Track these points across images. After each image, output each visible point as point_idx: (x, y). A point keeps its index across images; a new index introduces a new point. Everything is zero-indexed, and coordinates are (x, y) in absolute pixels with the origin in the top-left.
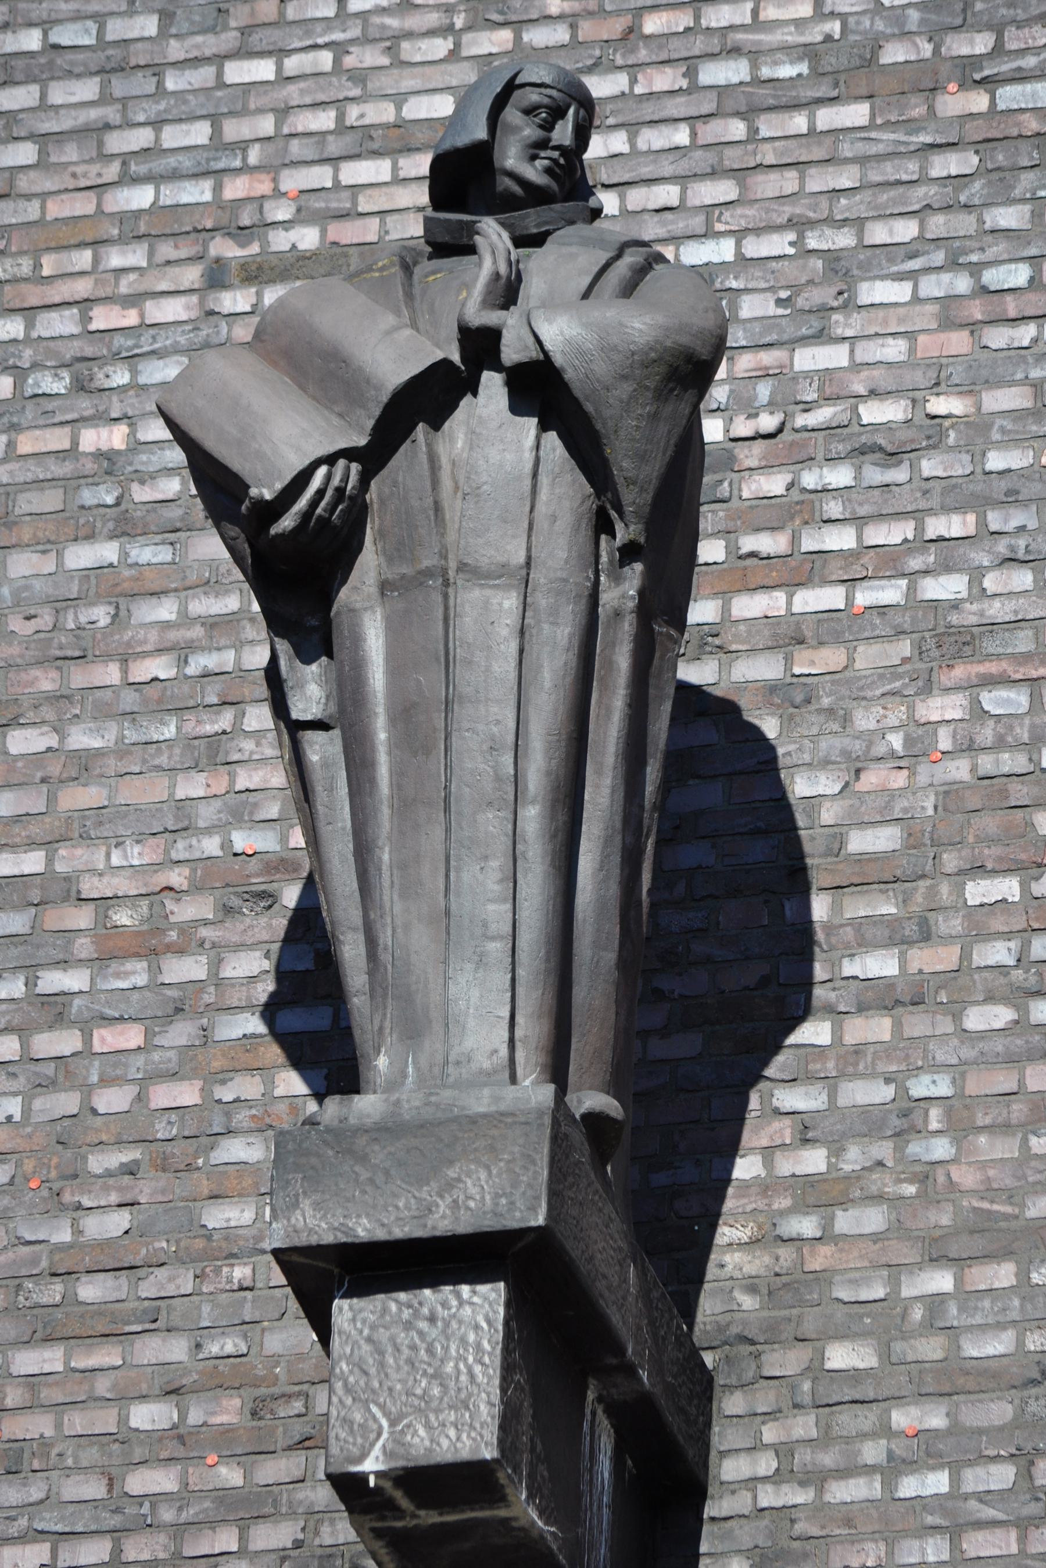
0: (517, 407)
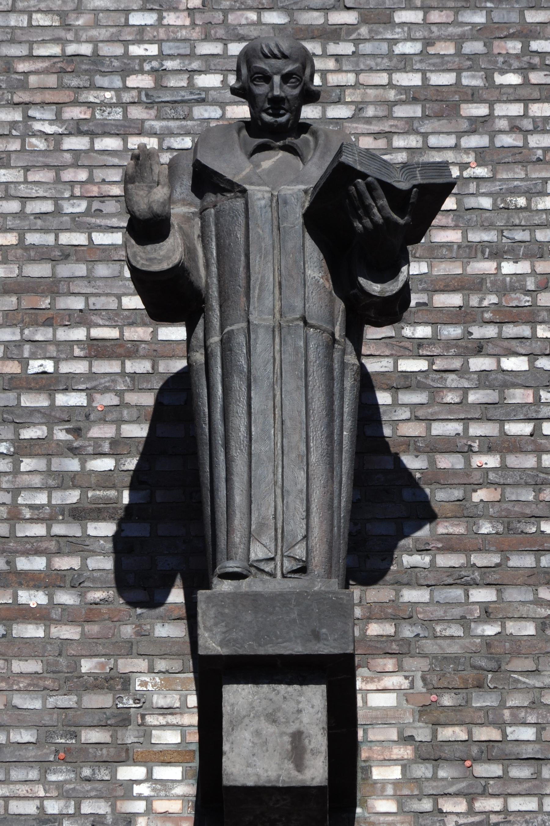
0: (133, 183)
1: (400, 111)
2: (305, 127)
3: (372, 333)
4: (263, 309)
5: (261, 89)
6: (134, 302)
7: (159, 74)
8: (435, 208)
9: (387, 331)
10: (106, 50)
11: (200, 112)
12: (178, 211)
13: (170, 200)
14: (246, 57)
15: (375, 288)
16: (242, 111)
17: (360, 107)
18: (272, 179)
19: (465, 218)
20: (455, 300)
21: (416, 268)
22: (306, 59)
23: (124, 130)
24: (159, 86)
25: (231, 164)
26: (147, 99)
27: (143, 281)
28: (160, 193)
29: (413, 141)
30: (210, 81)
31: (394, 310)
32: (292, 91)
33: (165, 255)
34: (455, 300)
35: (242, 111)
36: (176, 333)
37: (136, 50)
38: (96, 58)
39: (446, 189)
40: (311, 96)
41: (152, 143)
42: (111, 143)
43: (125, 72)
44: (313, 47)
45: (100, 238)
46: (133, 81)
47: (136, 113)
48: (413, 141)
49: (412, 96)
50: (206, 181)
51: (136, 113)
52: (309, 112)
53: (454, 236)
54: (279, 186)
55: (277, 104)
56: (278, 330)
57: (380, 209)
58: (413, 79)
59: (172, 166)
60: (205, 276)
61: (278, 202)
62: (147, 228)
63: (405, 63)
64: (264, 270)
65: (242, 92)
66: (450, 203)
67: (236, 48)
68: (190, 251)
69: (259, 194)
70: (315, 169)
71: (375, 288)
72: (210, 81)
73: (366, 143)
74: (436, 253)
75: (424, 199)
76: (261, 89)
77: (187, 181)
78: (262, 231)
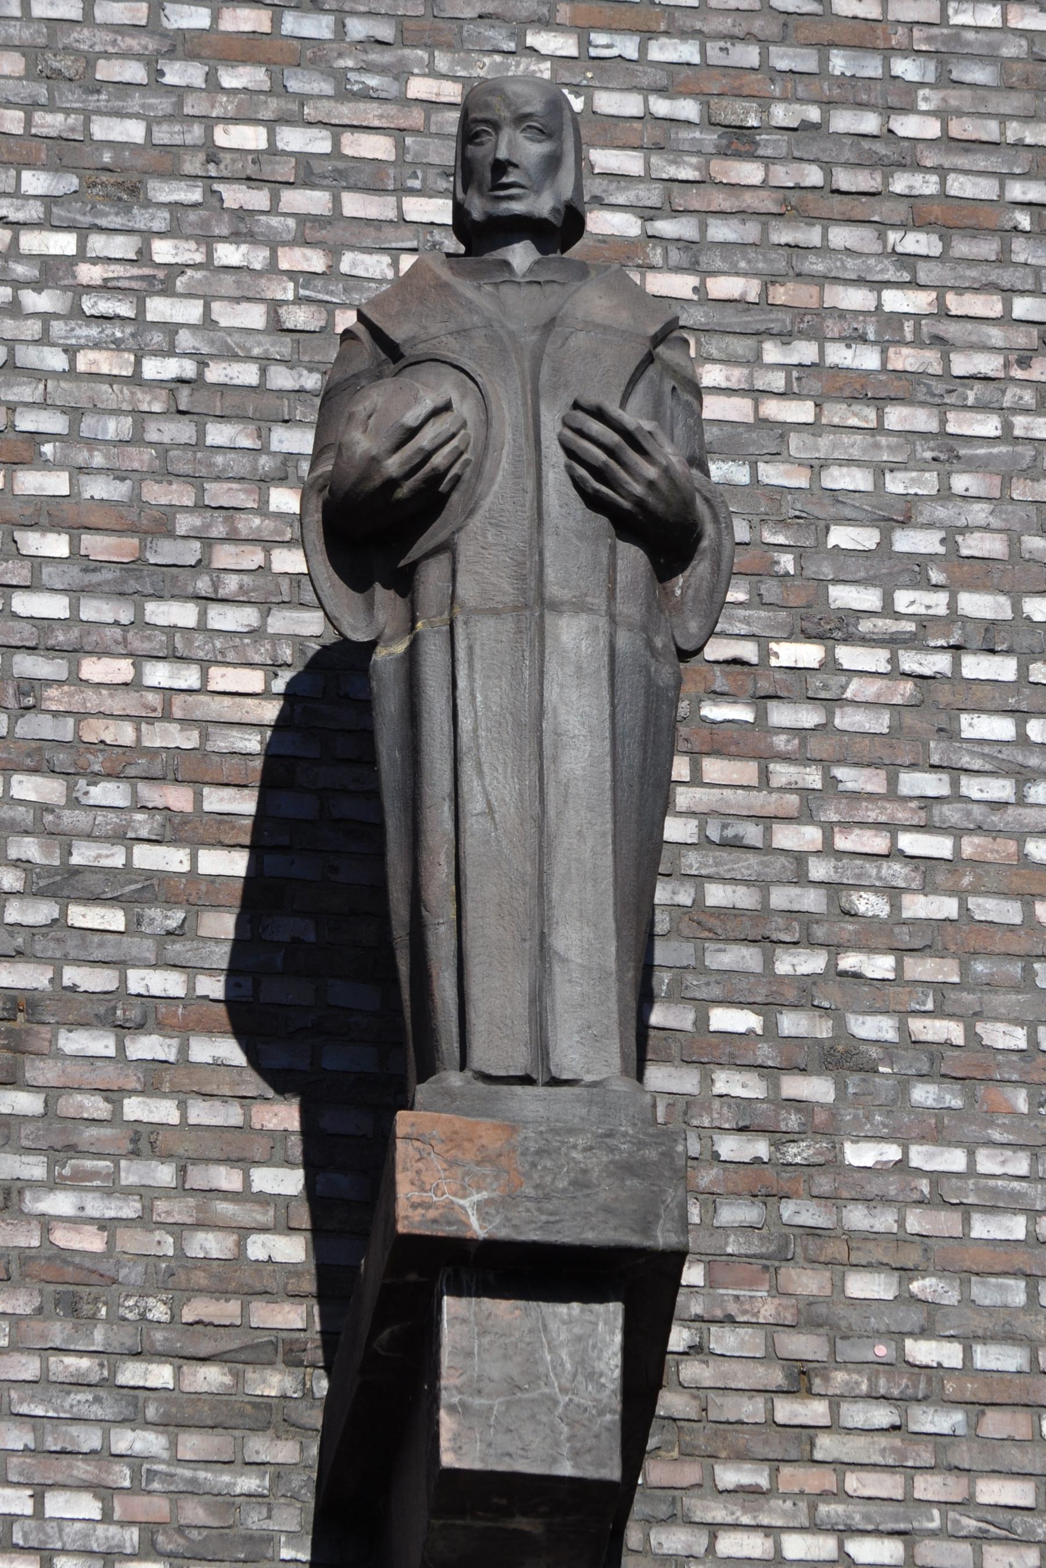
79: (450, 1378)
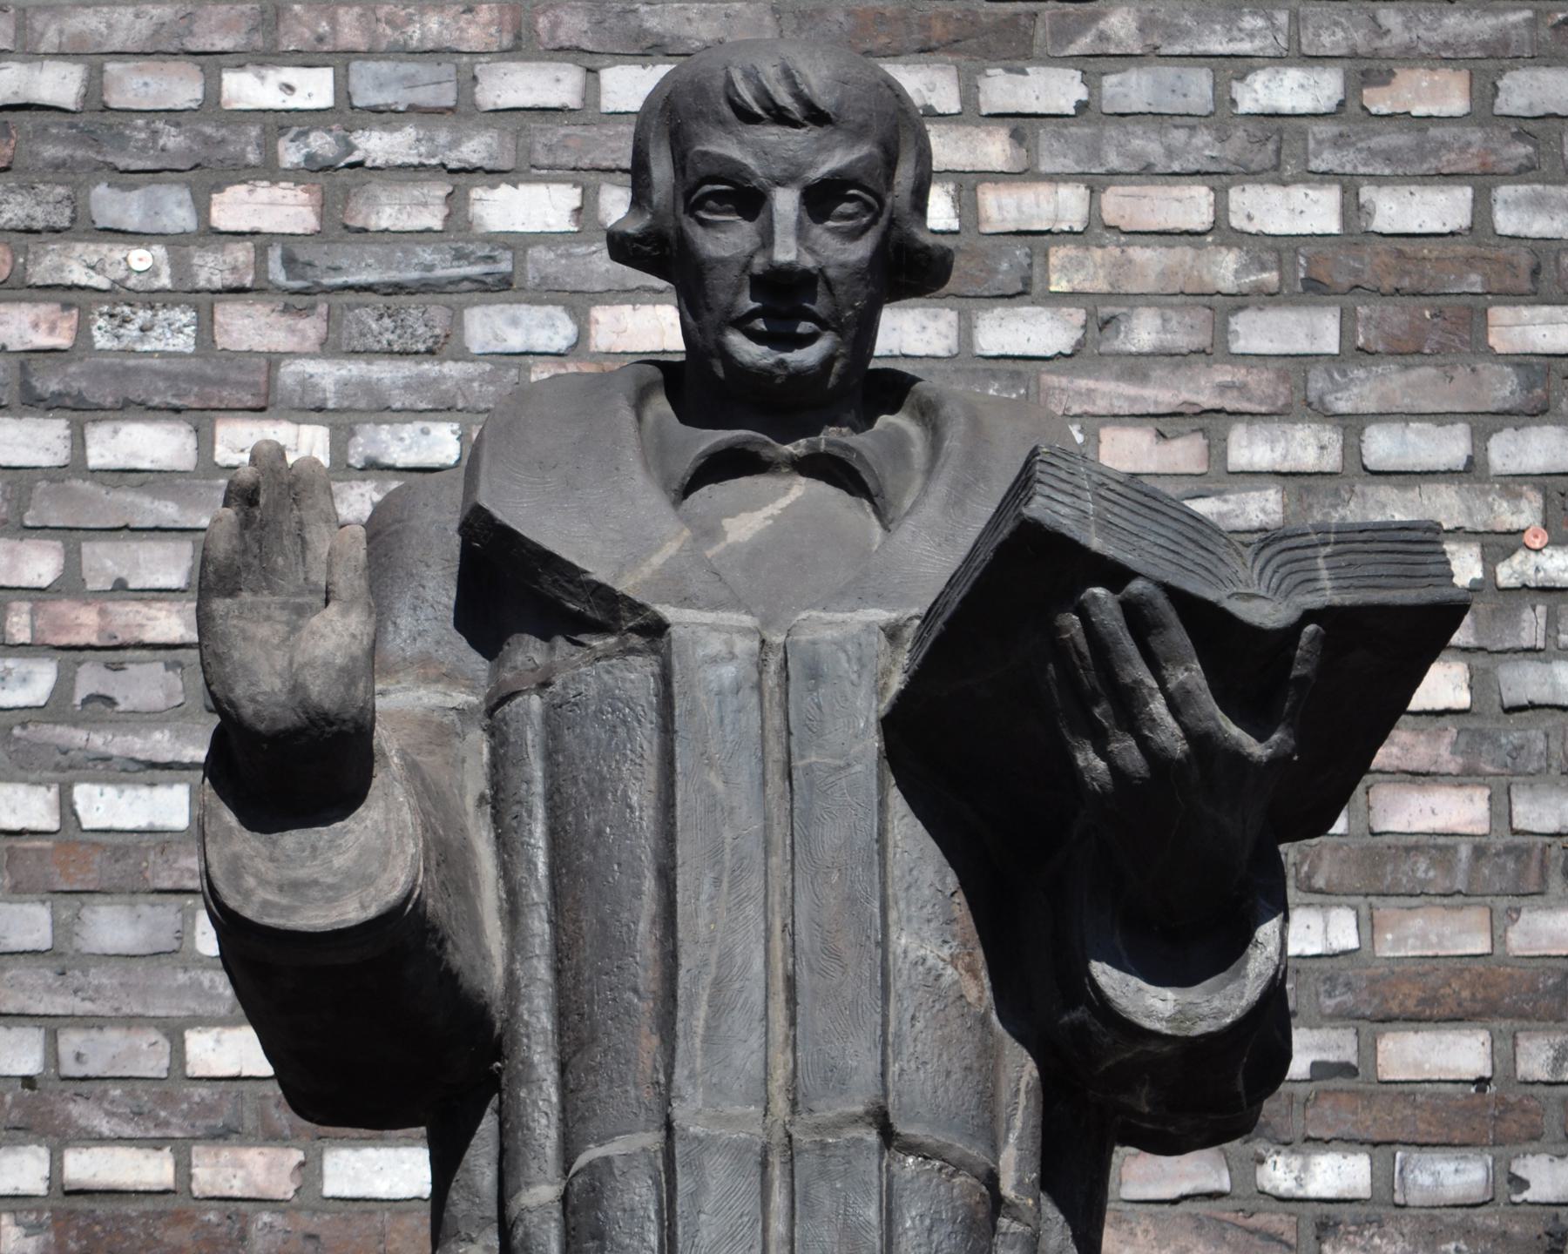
1: (1258, 333)
2: (891, 389)
3: (1139, 1175)
4: (725, 1082)
5: (724, 240)
6: (233, 1051)
7: (337, 178)
8: (1387, 703)
9: (1198, 1171)
10: (135, 87)
11: (493, 327)
12: (402, 705)
13: (371, 661)
14: (670, 116)
15: (1153, 1005)
16: (653, 326)
17: (1102, 315)
18: (760, 581)
19: (1496, 741)
20: (1462, 1054)
21: (1314, 931)
22: (899, 129)
23: (196, 395)
24: (338, 228)
25: (612, 524)
26: (293, 277)
27: (269, 970)
28: (335, 634)
29: (1307, 447)
30: (531, 208)
31: (1222, 1089)
32: (842, 251)
33: (342, 874)
34: (1462, 1054)
35: (653, 326)
36: (394, 1169)
37: (248, 89)
38: (96, 118)
39: (1427, 629)
40: (913, 269)
41: (307, 443)
42: (153, 444)
43: (207, 173)
44: (926, 84)
45: (105, 807)
46: (237, 208)
47: (247, 328)
48: (1307, 447)
49: (1303, 273)
50: (509, 589)
51: (247, 328)
52: (908, 332)
53: (1458, 811)
54: (796, 606)
55: (784, 297)
56: (779, 1159)
57: (1176, 704)
58: (1311, 211)
59: (382, 531)
60: (503, 952)
61: (783, 671)
62: (285, 768)
63: (1277, 148)
64: (729, 933)
65: (654, 252)
66: (1443, 685)
67: (629, 87)
68: (446, 856)
69: (713, 641)
70: (930, 546)
71: (1153, 1005)
72: (531, 208)
73: (1127, 451)
74: (1389, 875)
75: (1345, 671)
76: (724, 240)
77: (438, 588)
78: (725, 787)
79: (1110, 993)
